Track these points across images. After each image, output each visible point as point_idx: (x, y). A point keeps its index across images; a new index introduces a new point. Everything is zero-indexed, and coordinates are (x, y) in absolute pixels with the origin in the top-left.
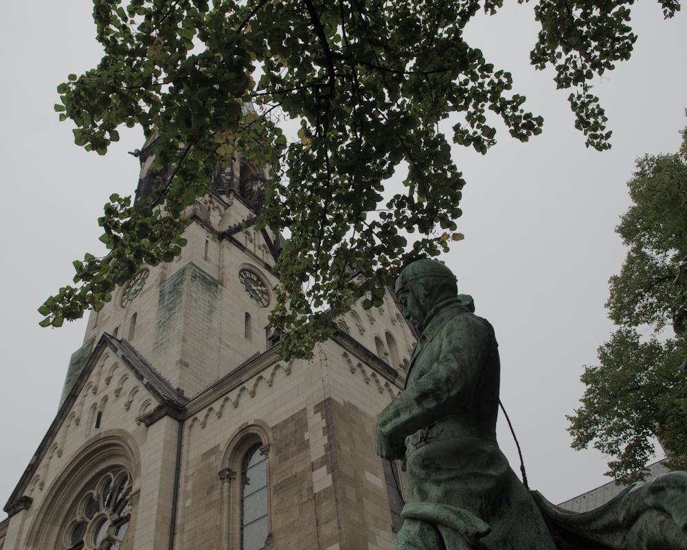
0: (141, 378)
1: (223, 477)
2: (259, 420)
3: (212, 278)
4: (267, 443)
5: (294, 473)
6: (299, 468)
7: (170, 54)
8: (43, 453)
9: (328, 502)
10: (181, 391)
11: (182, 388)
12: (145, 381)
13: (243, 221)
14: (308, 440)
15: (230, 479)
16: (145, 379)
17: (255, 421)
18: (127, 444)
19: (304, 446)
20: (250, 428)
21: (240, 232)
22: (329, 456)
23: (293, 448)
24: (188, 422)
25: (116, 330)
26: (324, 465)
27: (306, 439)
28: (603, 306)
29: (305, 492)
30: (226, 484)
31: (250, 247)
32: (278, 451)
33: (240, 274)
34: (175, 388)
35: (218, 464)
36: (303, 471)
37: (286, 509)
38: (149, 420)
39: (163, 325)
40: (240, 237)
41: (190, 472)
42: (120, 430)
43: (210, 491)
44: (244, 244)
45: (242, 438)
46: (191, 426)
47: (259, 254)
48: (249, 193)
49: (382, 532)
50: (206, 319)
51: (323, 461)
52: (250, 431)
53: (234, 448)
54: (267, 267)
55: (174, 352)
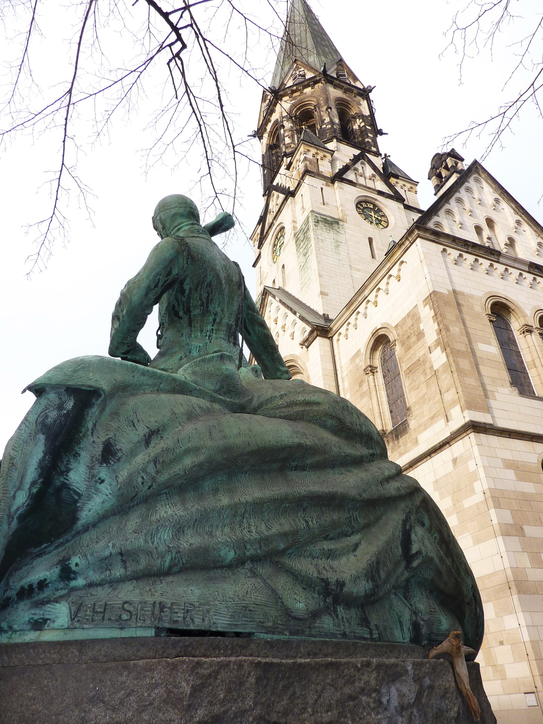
0: (295, 313)
1: (367, 372)
2: (385, 323)
3: (333, 218)
4: (393, 339)
5: (418, 358)
6: (420, 354)
9: (446, 375)
10: (326, 316)
11: (326, 313)
12: (298, 314)
13: (350, 160)
14: (423, 330)
15: (373, 373)
16: (297, 313)
17: (382, 324)
18: (298, 364)
19: (420, 335)
20: (379, 331)
21: (349, 171)
22: (441, 338)
23: (413, 339)
24: (335, 338)
25: (274, 281)
26: (438, 346)
27: (422, 329)
29: (428, 371)
30: (371, 377)
31: (361, 181)
32: (403, 344)
33: (357, 207)
34: (321, 314)
35: (363, 362)
36: (424, 355)
37: (417, 387)
38: (307, 343)
39: (303, 268)
40: (350, 175)
41: (345, 374)
42: (291, 355)
43: (360, 386)
44: (355, 181)
45: (375, 340)
46: (338, 340)
47: (370, 184)
48: (352, 133)
49: (500, 389)
50: (335, 254)
51: (438, 343)
52: (379, 334)
53: (371, 349)
54: (380, 193)
55: (316, 288)
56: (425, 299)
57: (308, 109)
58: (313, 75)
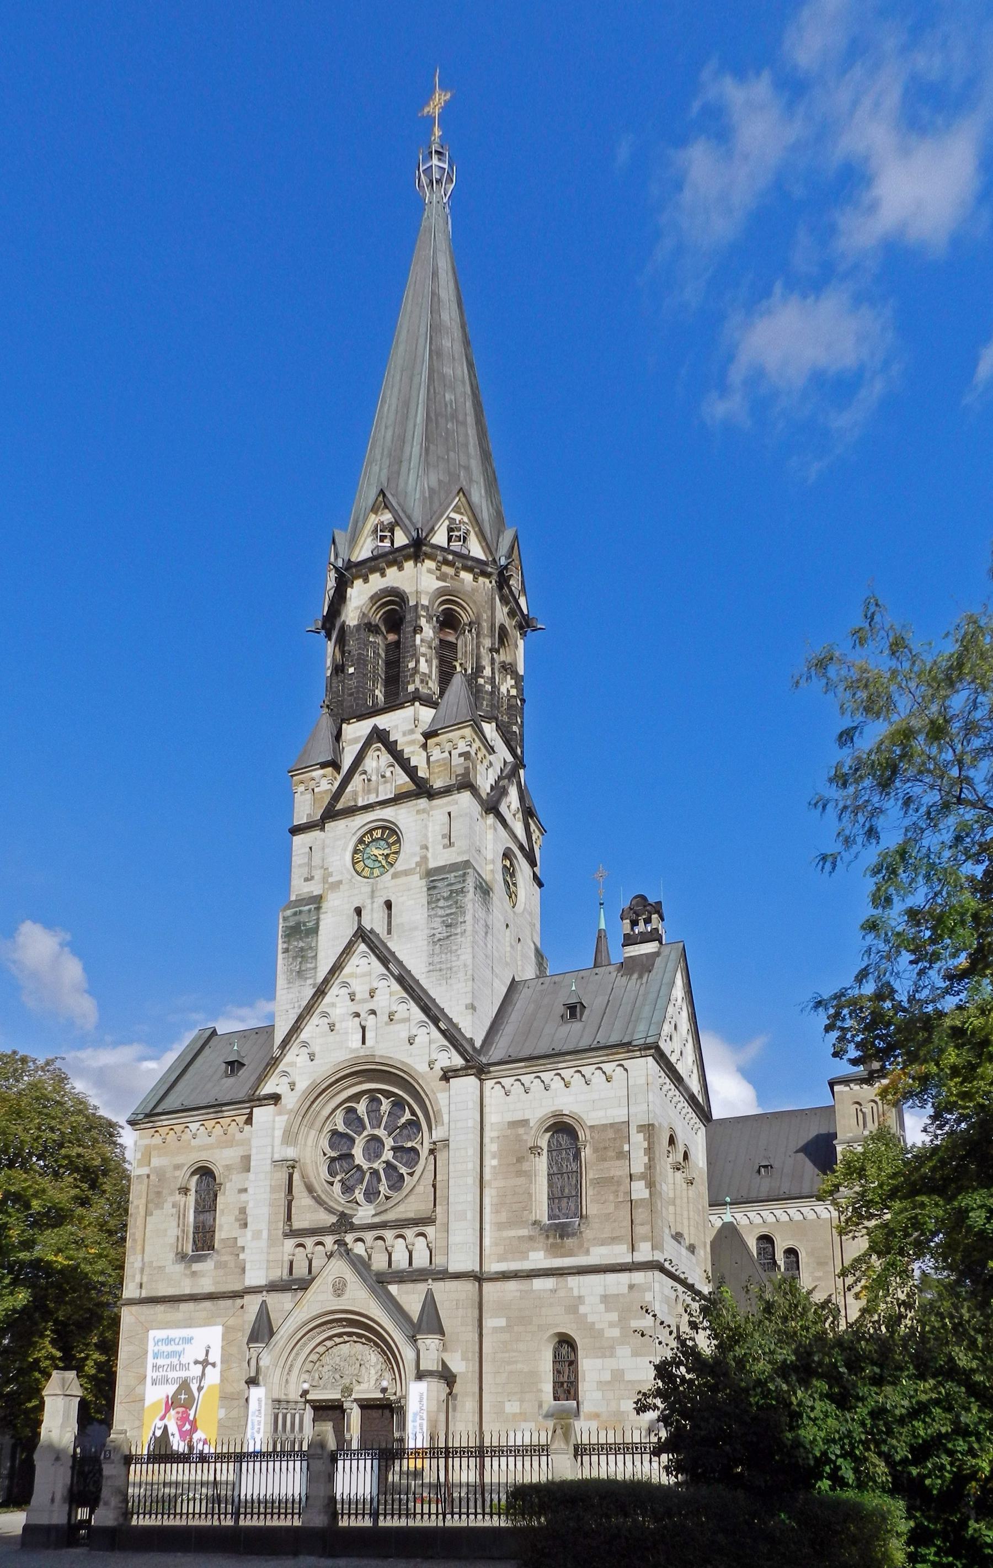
7: (893, 1027)
8: (288, 1048)
17: (571, 1112)
28: (384, 579)
29: (621, 1194)
51: (642, 1177)
56: (642, 1126)
57: (459, 614)
58: (483, 557)
